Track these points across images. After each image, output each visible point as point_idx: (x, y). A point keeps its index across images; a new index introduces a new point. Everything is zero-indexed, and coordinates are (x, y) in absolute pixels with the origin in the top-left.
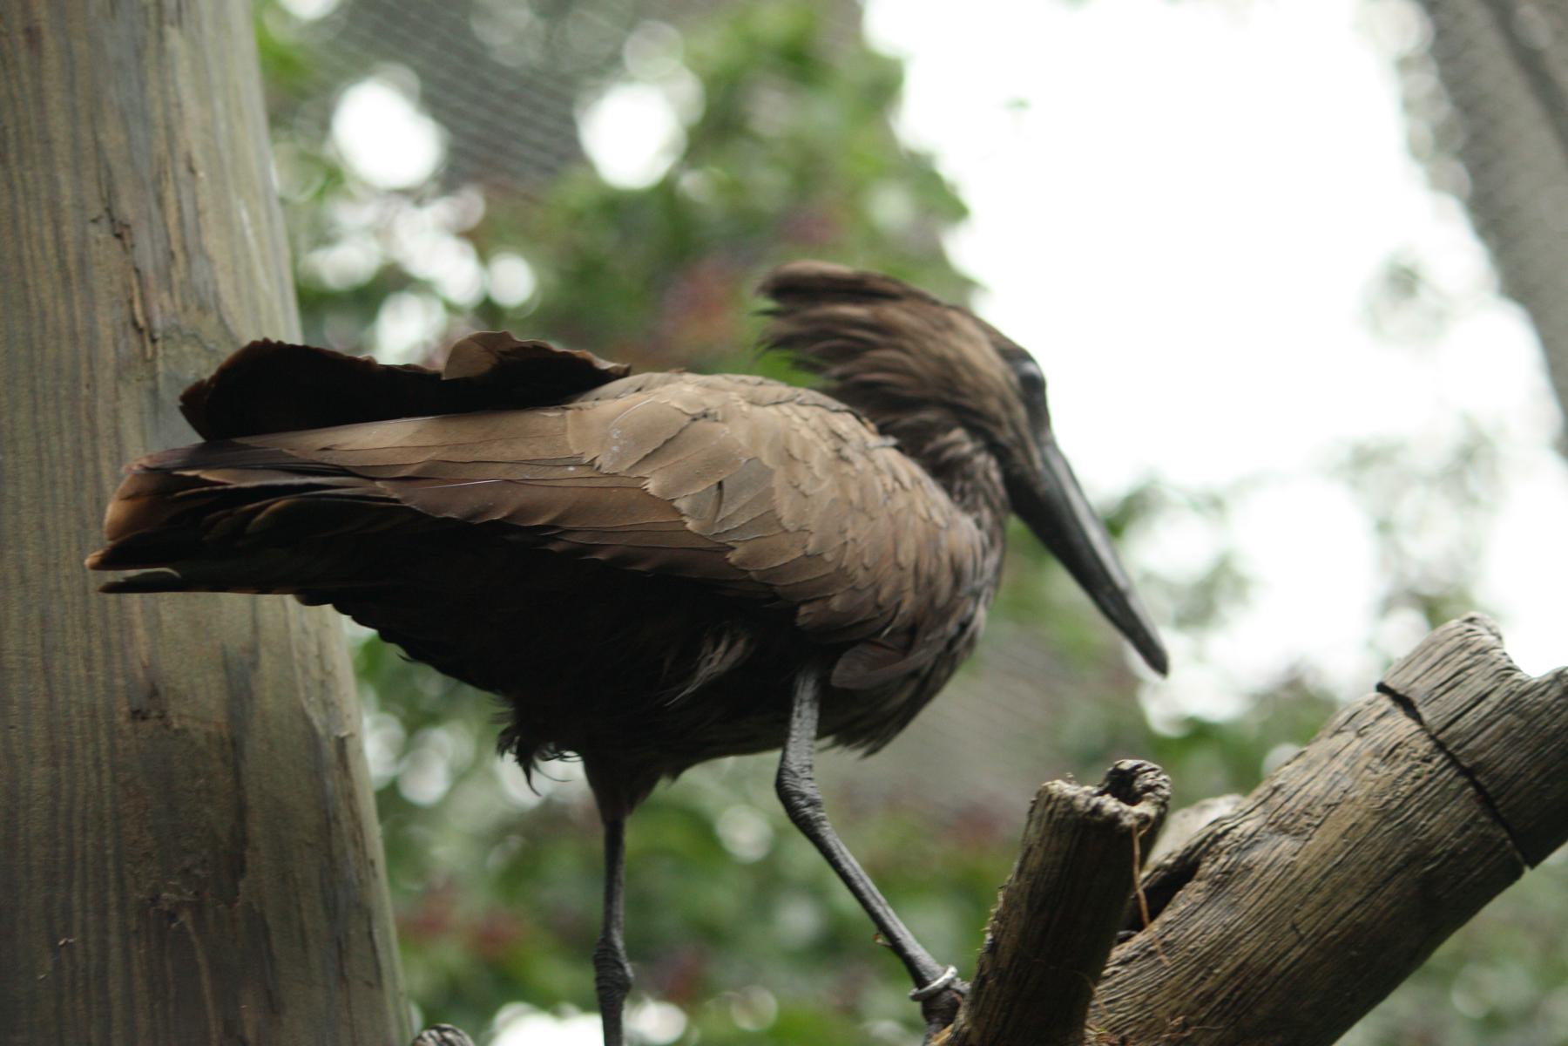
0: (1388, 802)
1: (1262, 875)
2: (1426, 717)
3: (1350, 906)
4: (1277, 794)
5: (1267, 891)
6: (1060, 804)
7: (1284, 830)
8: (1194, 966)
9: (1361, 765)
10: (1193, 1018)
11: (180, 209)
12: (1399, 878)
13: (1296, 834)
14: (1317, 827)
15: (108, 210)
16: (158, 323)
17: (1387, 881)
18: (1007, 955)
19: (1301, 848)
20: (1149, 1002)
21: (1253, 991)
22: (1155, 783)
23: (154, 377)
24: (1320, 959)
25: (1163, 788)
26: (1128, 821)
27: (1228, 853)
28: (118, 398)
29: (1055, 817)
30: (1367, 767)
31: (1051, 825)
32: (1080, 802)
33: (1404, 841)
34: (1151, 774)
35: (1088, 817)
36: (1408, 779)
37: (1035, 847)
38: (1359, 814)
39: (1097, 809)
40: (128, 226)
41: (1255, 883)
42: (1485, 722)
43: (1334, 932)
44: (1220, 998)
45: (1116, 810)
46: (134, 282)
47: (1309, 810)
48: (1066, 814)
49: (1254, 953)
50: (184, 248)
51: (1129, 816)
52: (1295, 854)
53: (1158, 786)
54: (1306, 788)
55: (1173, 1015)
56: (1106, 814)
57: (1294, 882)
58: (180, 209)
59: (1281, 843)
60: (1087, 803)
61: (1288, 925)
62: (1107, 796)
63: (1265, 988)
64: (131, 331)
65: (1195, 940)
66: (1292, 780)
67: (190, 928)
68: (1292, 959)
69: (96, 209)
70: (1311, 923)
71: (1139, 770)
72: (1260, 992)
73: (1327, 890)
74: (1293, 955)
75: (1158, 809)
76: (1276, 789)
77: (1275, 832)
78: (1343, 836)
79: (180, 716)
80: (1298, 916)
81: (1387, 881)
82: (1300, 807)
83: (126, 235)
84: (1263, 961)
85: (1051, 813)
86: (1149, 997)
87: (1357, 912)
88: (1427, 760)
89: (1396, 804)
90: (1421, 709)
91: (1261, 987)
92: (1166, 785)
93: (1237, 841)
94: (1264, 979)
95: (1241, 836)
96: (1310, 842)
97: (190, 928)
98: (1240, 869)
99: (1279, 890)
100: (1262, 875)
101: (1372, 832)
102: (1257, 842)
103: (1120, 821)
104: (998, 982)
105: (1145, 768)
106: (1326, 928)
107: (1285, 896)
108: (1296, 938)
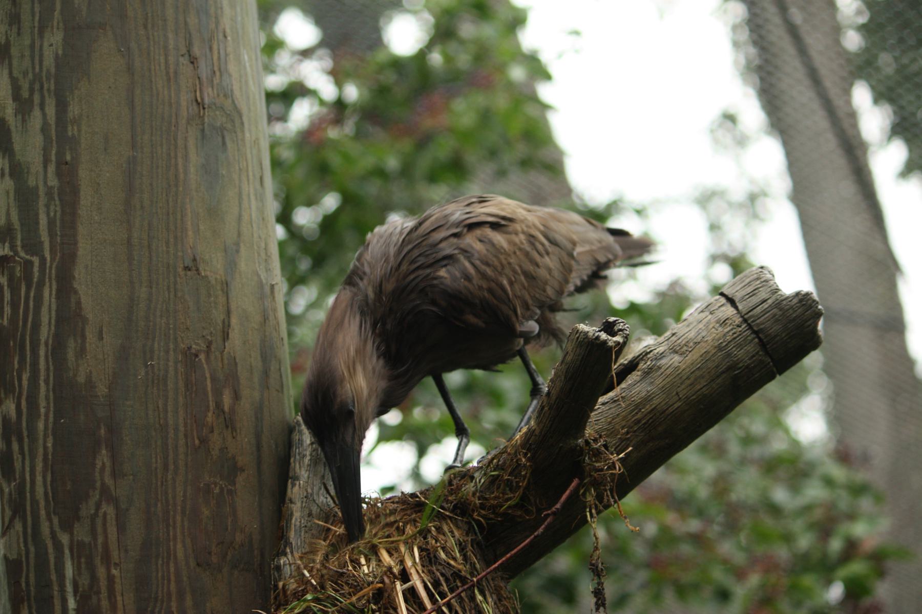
0: (721, 343)
2: (740, 308)
3: (702, 386)
5: (667, 378)
6: (582, 334)
7: (676, 352)
8: (633, 408)
9: (711, 326)
10: (631, 430)
11: (219, 53)
12: (724, 376)
13: (681, 354)
15: (189, 51)
16: (206, 101)
17: (718, 377)
18: (554, 398)
19: (683, 360)
20: (613, 422)
22: (623, 328)
23: (203, 124)
25: (627, 330)
26: (610, 344)
27: (651, 360)
28: (187, 132)
30: (713, 327)
31: (577, 343)
32: (591, 334)
33: (727, 360)
34: (622, 324)
35: (593, 341)
36: (731, 334)
37: (570, 352)
38: (708, 347)
39: (598, 337)
40: (196, 59)
41: (662, 374)
42: (765, 312)
43: (694, 397)
44: (643, 422)
45: (606, 338)
47: (687, 344)
48: (584, 339)
50: (220, 69)
51: (611, 341)
52: (680, 363)
53: (624, 329)
54: (687, 335)
55: (623, 428)
56: (602, 340)
57: (679, 374)
58: (219, 53)
59: (674, 358)
60: (594, 335)
61: (675, 393)
62: (602, 332)
63: (662, 419)
64: (195, 103)
65: (635, 396)
67: (203, 361)
69: (183, 50)
71: (617, 322)
72: (660, 420)
74: (676, 406)
75: (624, 339)
77: (672, 352)
78: (701, 356)
80: (679, 389)
81: (718, 377)
82: (683, 342)
85: (578, 338)
86: (613, 419)
87: (704, 389)
88: (739, 326)
89: (724, 344)
90: (738, 304)
92: (628, 329)
94: (663, 415)
95: (657, 353)
96: (687, 358)
97: (203, 361)
98: (656, 367)
99: (672, 377)
101: (713, 355)
102: (664, 356)
103: (608, 343)
104: (549, 409)
105: (619, 321)
108: (678, 398)
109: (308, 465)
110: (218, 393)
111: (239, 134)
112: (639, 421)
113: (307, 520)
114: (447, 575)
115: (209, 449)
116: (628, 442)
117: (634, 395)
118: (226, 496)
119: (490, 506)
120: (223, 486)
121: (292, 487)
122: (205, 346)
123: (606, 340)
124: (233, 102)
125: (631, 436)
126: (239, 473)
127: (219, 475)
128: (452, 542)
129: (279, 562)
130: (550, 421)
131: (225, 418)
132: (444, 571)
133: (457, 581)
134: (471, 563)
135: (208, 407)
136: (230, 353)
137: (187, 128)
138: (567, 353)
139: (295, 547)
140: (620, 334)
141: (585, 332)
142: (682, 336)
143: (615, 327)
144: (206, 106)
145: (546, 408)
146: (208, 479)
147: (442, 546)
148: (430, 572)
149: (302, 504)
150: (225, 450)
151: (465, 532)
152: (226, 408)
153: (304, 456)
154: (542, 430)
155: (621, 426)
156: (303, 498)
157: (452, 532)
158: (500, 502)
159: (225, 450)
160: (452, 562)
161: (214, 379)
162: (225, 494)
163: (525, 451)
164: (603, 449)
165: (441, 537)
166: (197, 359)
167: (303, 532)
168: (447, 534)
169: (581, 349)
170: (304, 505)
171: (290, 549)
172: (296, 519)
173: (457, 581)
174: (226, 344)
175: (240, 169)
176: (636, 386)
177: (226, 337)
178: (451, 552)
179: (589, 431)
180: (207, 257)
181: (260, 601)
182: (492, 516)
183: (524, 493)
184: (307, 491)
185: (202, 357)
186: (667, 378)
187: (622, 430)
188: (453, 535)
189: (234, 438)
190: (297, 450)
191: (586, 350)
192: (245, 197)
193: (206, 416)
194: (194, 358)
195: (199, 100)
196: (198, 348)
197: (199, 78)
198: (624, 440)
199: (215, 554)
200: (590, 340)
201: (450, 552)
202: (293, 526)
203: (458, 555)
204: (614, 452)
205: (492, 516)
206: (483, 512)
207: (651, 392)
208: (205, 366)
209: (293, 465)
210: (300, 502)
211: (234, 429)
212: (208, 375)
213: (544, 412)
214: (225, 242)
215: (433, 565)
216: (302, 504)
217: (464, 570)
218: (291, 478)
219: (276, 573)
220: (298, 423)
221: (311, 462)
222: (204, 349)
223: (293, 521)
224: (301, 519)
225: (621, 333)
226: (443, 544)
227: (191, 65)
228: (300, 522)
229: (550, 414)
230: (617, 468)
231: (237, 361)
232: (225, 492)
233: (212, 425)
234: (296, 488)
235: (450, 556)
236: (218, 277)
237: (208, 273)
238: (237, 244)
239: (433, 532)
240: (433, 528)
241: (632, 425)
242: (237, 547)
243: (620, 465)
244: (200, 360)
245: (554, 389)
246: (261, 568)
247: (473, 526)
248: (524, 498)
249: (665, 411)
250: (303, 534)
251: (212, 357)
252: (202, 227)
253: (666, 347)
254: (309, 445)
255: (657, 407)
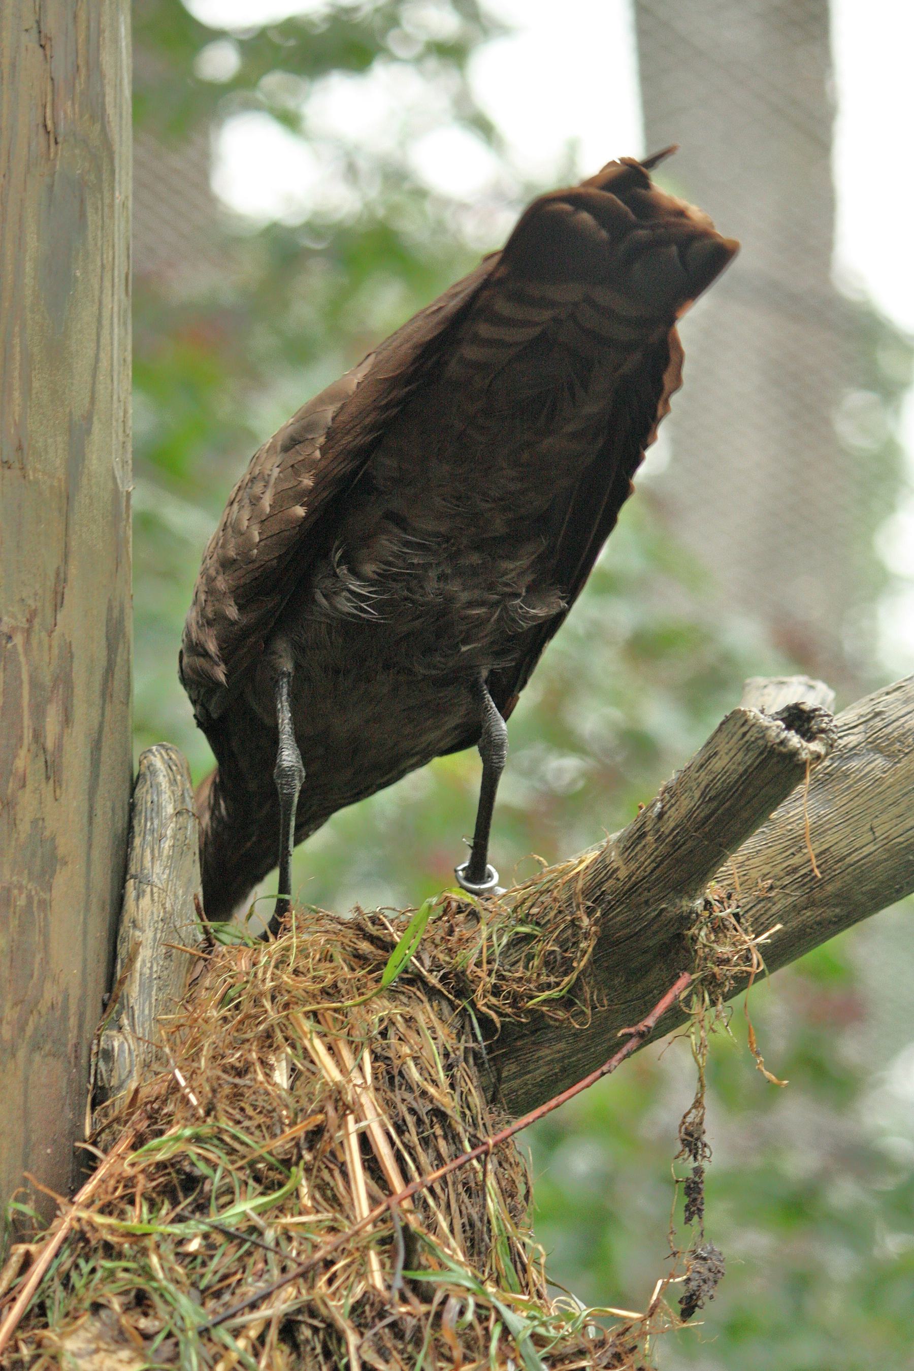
1: (856, 783)
4: (878, 719)
5: (857, 796)
6: (754, 729)
7: (878, 749)
8: (788, 843)
10: (778, 883)
11: (88, 28)
13: (888, 756)
14: (907, 754)
15: (38, 22)
16: (62, 129)
19: (890, 769)
20: (746, 863)
21: (829, 871)
23: (52, 175)
24: (885, 857)
26: (804, 755)
27: (832, 759)
28: (25, 190)
29: (747, 738)
31: (742, 742)
34: (826, 719)
35: (775, 746)
40: (50, 39)
41: (849, 788)
44: (802, 872)
45: (799, 746)
46: (49, 89)
47: (902, 739)
49: (128, 249)
50: (87, 63)
51: (806, 751)
52: (885, 772)
53: (830, 730)
54: (903, 720)
55: (764, 877)
56: (791, 748)
57: (880, 793)
58: (88, 28)
59: (875, 760)
60: (778, 735)
61: (868, 826)
63: (837, 872)
64: (41, 130)
65: (793, 822)
66: (891, 709)
67: (20, 649)
68: (865, 854)
69: (30, 22)
70: (886, 829)
72: (834, 873)
73: (903, 807)
74: (866, 851)
76: (878, 714)
77: (872, 750)
79: (35, 470)
80: (876, 822)
82: (895, 734)
83: (48, 47)
84: (842, 851)
86: (748, 859)
91: (835, 870)
93: (840, 750)
94: (840, 864)
95: (845, 746)
96: (898, 765)
97: (20, 649)
98: (839, 774)
99: (866, 798)
100: (856, 783)
102: (855, 754)
103: (799, 754)
106: (895, 835)
107: (870, 803)
108: (872, 838)
109: (169, 857)
110: (39, 712)
111: (107, 194)
112: (795, 870)
113: (162, 966)
114: (420, 1112)
115: (15, 819)
116: (769, 905)
117: (791, 820)
118: (36, 914)
119: (509, 992)
120: (33, 893)
121: (138, 898)
122: (25, 620)
123: (798, 749)
124: (104, 131)
125: (778, 893)
126: (58, 867)
127: (26, 871)
128: (432, 1050)
129: (109, 1042)
130: (652, 862)
131: (46, 762)
132: (415, 1105)
133: (437, 1126)
134: (462, 1093)
135: (21, 738)
136: (63, 635)
137: (25, 182)
138: (716, 754)
139: (138, 1018)
140: (821, 739)
141: (761, 727)
142: (894, 721)
143: (813, 722)
144: (60, 139)
145: (650, 838)
146: (8, 877)
147: (415, 1055)
148: (389, 1104)
149: (155, 934)
150: (41, 822)
151: (455, 1031)
152: (50, 744)
153: (161, 838)
154: (630, 877)
155: (760, 873)
156: (157, 922)
157: (432, 1029)
158: (530, 990)
159: (41, 822)
160: (432, 1090)
161: (35, 684)
162: (35, 909)
163: (589, 904)
164: (733, 920)
165: (413, 1038)
166: (9, 645)
167: (155, 988)
168: (423, 1031)
169: (746, 755)
170: (158, 936)
171: (128, 1019)
172: (144, 961)
173: (437, 1126)
174: (58, 617)
175: (103, 266)
176: (797, 803)
177: (59, 601)
178: (430, 1069)
179: (713, 890)
180: (40, 444)
181: (71, 1116)
182: (509, 1010)
183: (578, 978)
184: (165, 908)
185: (18, 639)
186: (857, 796)
187: (763, 881)
188: (435, 1036)
189: (56, 800)
190: (149, 824)
191: (757, 758)
192: (106, 322)
193: (15, 756)
194: (4, 642)
195: (49, 123)
196: (13, 623)
197: (52, 79)
198: (763, 900)
199: (8, 1023)
200: (770, 744)
201: (427, 1069)
202: (137, 975)
203: (442, 1074)
204: (750, 929)
205: (509, 1010)
206: (494, 1000)
207: (825, 819)
208: (22, 659)
209: (137, 851)
210: (153, 929)
211: (58, 783)
212: (25, 677)
213: (643, 843)
214: (71, 413)
215: (397, 1091)
216: (155, 934)
217: (450, 1104)
218: (134, 877)
219: (101, 1064)
220: (151, 768)
221: (173, 852)
222: (22, 625)
223: (138, 964)
224: (151, 962)
225: (823, 736)
226: (416, 1052)
227: (41, 50)
228: (151, 968)
229: (657, 848)
230: (755, 961)
231: (74, 649)
232: (35, 905)
233: (25, 774)
234: (145, 902)
235: (427, 1076)
236: (56, 484)
237: (40, 476)
238: (88, 418)
239: (398, 1025)
240: (399, 1017)
241: (782, 874)
242: (44, 1011)
243: (760, 956)
244: (15, 646)
245: (673, 809)
246: (76, 1051)
247: (470, 1015)
248: (575, 989)
249: (844, 858)
250: (154, 993)
251: (34, 642)
252: (36, 384)
253: (860, 738)
254: (171, 817)
255: (832, 849)
